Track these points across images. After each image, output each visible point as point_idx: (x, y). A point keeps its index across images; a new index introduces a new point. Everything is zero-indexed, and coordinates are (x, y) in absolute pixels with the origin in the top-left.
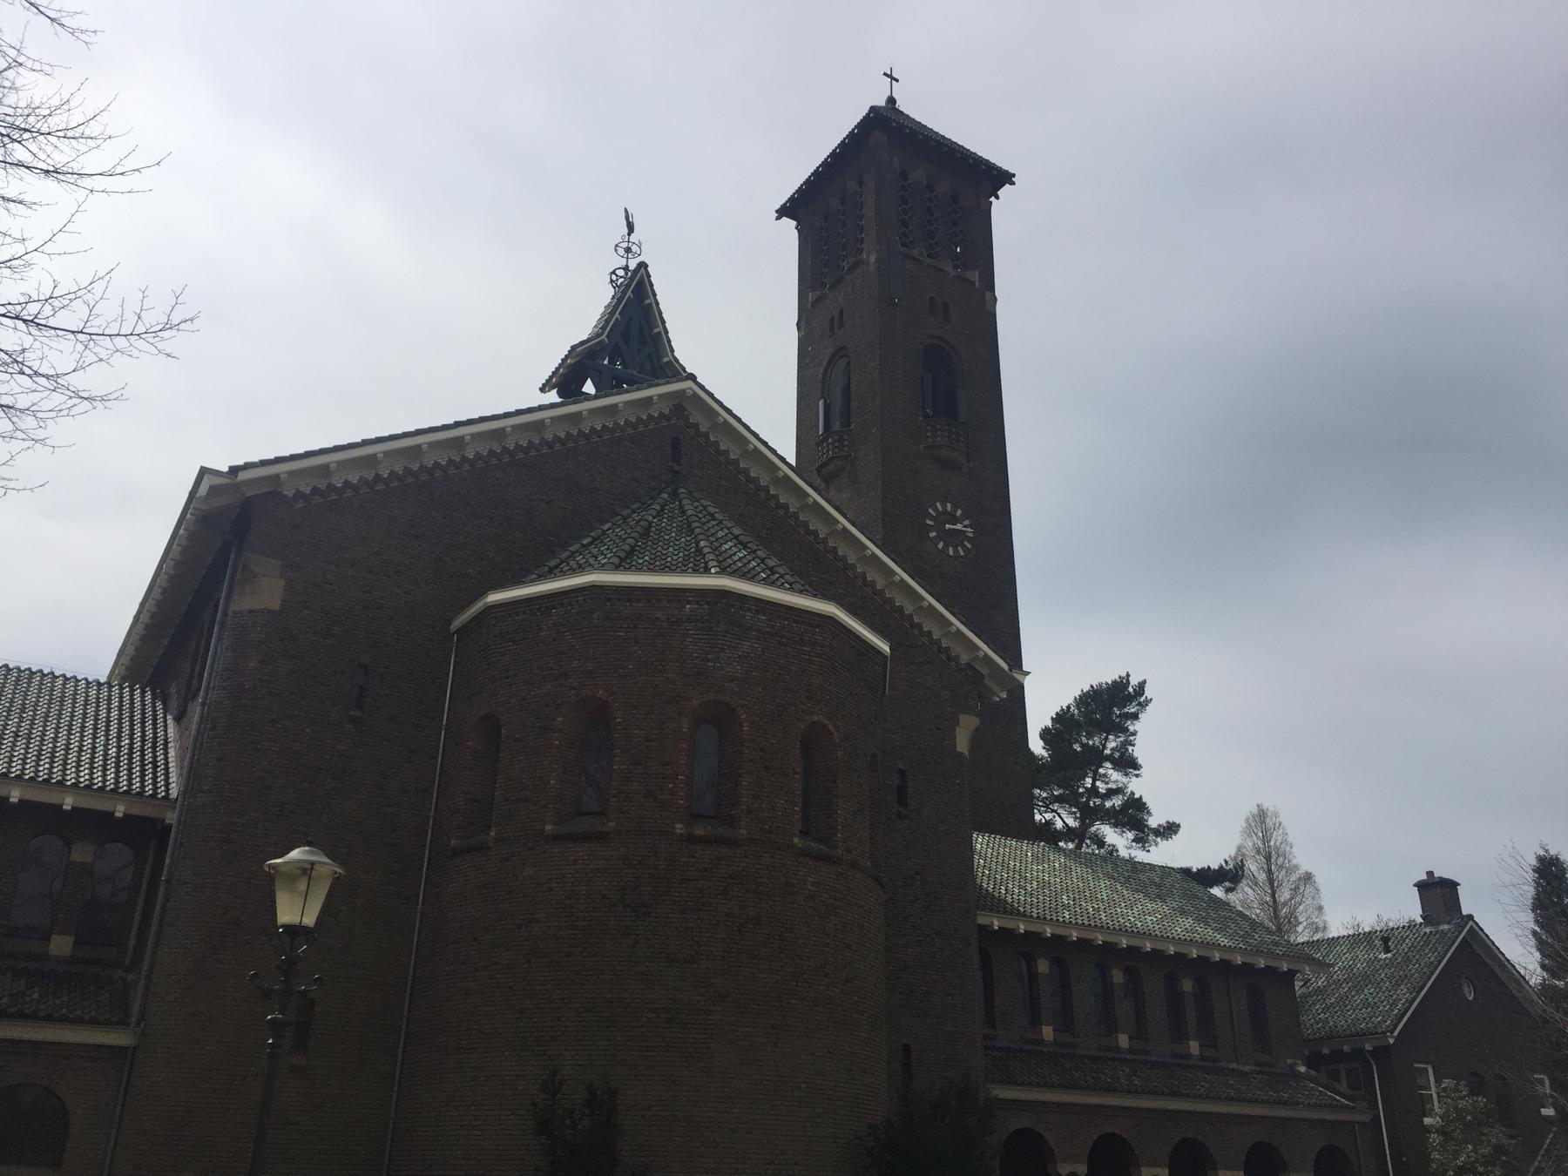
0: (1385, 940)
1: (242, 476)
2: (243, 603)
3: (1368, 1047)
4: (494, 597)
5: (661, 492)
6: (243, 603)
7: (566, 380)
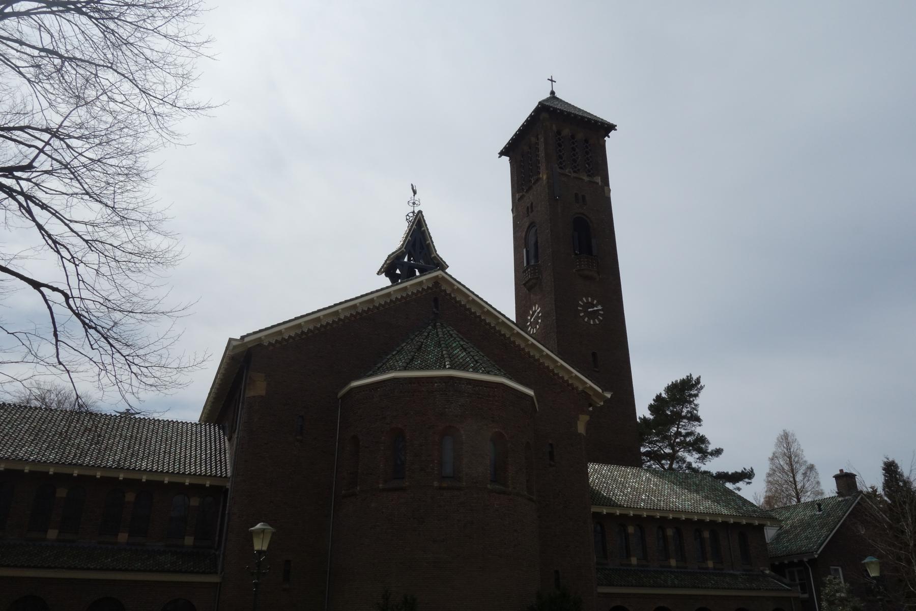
0: (819, 505)
1: (246, 340)
2: (250, 393)
3: (805, 560)
4: (355, 384)
5: (429, 325)
6: (250, 393)
7: (389, 269)
